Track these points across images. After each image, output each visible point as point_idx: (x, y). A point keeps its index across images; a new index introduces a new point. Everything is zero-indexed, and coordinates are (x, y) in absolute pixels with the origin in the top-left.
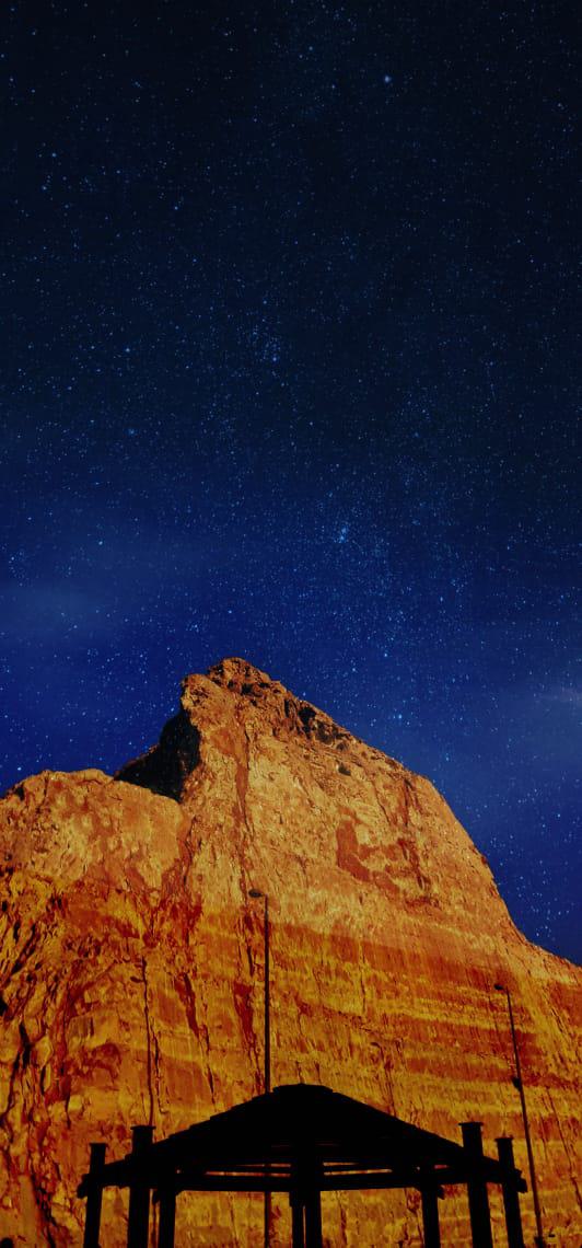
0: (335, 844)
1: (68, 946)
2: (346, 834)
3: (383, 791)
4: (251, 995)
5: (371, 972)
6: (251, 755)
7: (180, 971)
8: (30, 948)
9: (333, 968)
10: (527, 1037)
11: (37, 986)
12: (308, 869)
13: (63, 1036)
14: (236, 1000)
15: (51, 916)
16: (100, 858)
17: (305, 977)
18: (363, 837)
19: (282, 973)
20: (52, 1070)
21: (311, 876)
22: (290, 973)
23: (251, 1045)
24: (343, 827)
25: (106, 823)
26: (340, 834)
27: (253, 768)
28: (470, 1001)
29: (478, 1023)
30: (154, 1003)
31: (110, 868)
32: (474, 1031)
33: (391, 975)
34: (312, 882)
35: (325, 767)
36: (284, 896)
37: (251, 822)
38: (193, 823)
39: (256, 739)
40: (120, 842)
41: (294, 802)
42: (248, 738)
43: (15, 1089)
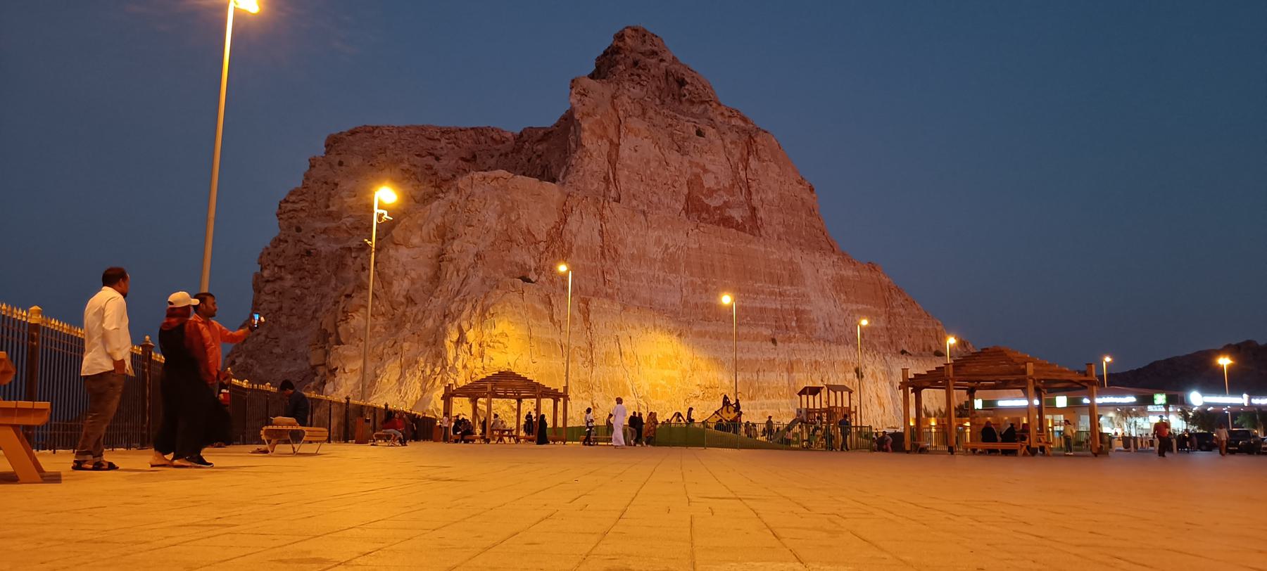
0: (686, 191)
1: (483, 281)
2: (694, 182)
3: (729, 146)
4: (589, 303)
5: (690, 279)
6: (622, 134)
7: (546, 293)
8: (464, 282)
9: (661, 278)
10: (803, 312)
11: (467, 305)
12: (649, 218)
13: (481, 329)
14: (579, 306)
15: (476, 263)
16: (505, 228)
17: (642, 285)
18: (709, 182)
19: (625, 283)
20: (476, 344)
21: (650, 222)
22: (631, 283)
23: (587, 328)
24: (693, 177)
25: (509, 204)
26: (689, 183)
27: (622, 144)
28: (763, 291)
29: (766, 305)
30: (529, 311)
31: (512, 234)
32: (762, 310)
33: (704, 280)
34: (651, 226)
35: (684, 132)
36: (630, 237)
37: (619, 184)
38: (568, 197)
39: (625, 122)
40: (519, 215)
41: (653, 164)
42: (620, 121)
43: (458, 353)
